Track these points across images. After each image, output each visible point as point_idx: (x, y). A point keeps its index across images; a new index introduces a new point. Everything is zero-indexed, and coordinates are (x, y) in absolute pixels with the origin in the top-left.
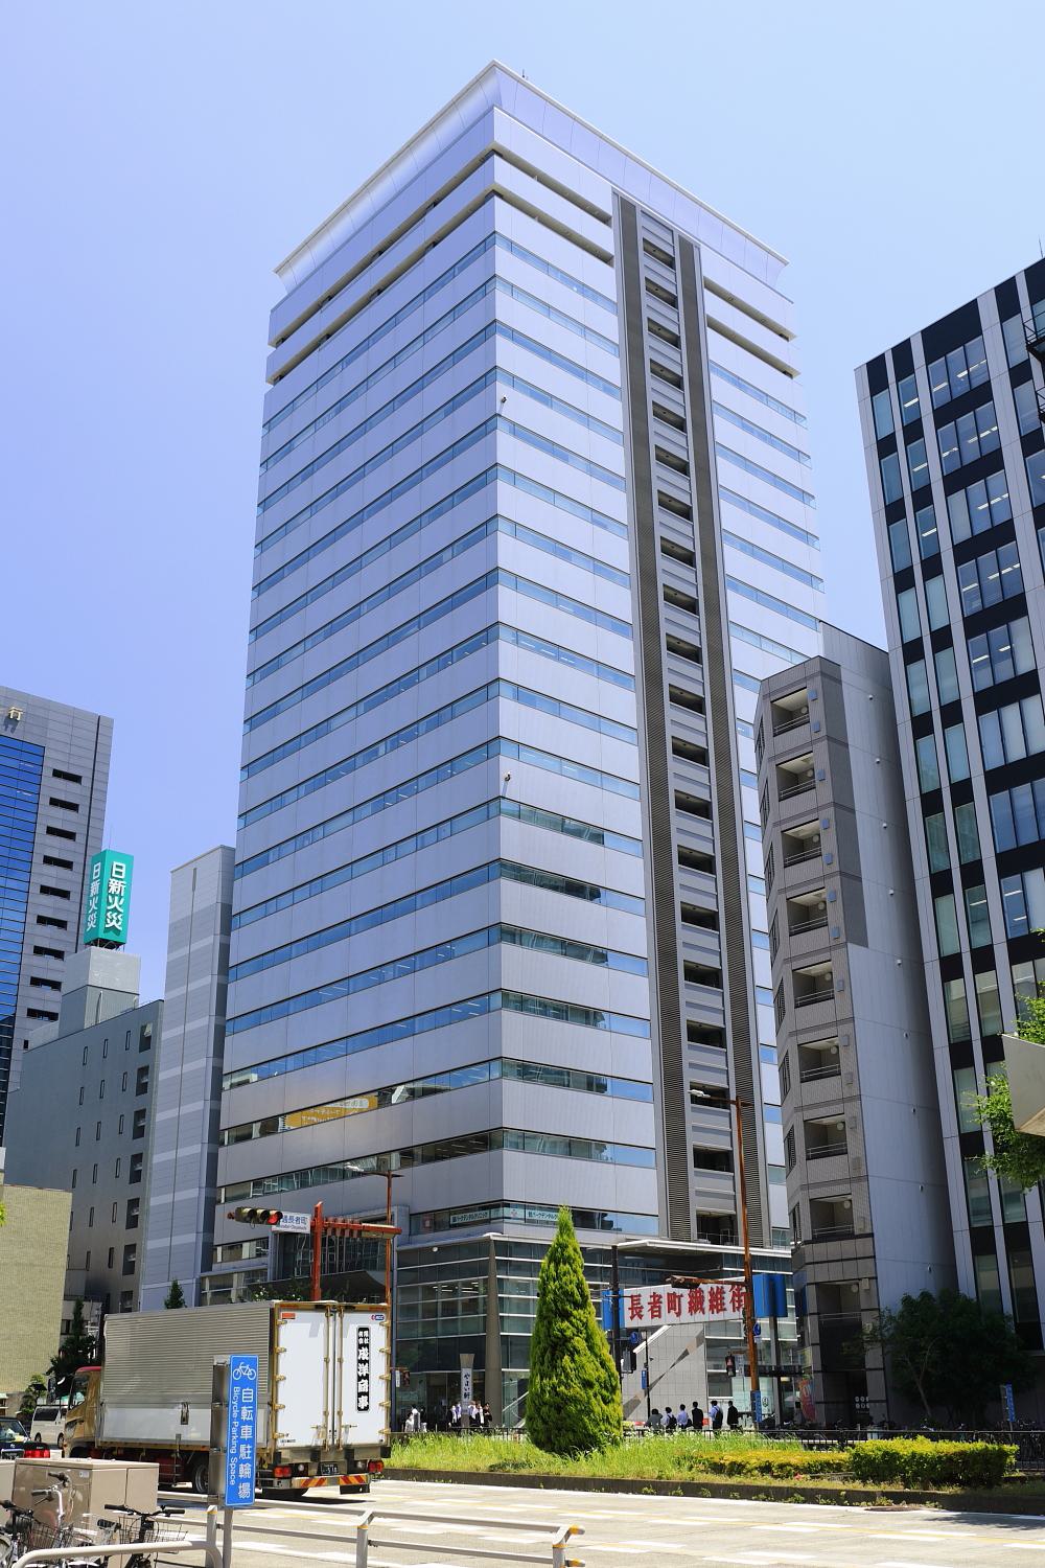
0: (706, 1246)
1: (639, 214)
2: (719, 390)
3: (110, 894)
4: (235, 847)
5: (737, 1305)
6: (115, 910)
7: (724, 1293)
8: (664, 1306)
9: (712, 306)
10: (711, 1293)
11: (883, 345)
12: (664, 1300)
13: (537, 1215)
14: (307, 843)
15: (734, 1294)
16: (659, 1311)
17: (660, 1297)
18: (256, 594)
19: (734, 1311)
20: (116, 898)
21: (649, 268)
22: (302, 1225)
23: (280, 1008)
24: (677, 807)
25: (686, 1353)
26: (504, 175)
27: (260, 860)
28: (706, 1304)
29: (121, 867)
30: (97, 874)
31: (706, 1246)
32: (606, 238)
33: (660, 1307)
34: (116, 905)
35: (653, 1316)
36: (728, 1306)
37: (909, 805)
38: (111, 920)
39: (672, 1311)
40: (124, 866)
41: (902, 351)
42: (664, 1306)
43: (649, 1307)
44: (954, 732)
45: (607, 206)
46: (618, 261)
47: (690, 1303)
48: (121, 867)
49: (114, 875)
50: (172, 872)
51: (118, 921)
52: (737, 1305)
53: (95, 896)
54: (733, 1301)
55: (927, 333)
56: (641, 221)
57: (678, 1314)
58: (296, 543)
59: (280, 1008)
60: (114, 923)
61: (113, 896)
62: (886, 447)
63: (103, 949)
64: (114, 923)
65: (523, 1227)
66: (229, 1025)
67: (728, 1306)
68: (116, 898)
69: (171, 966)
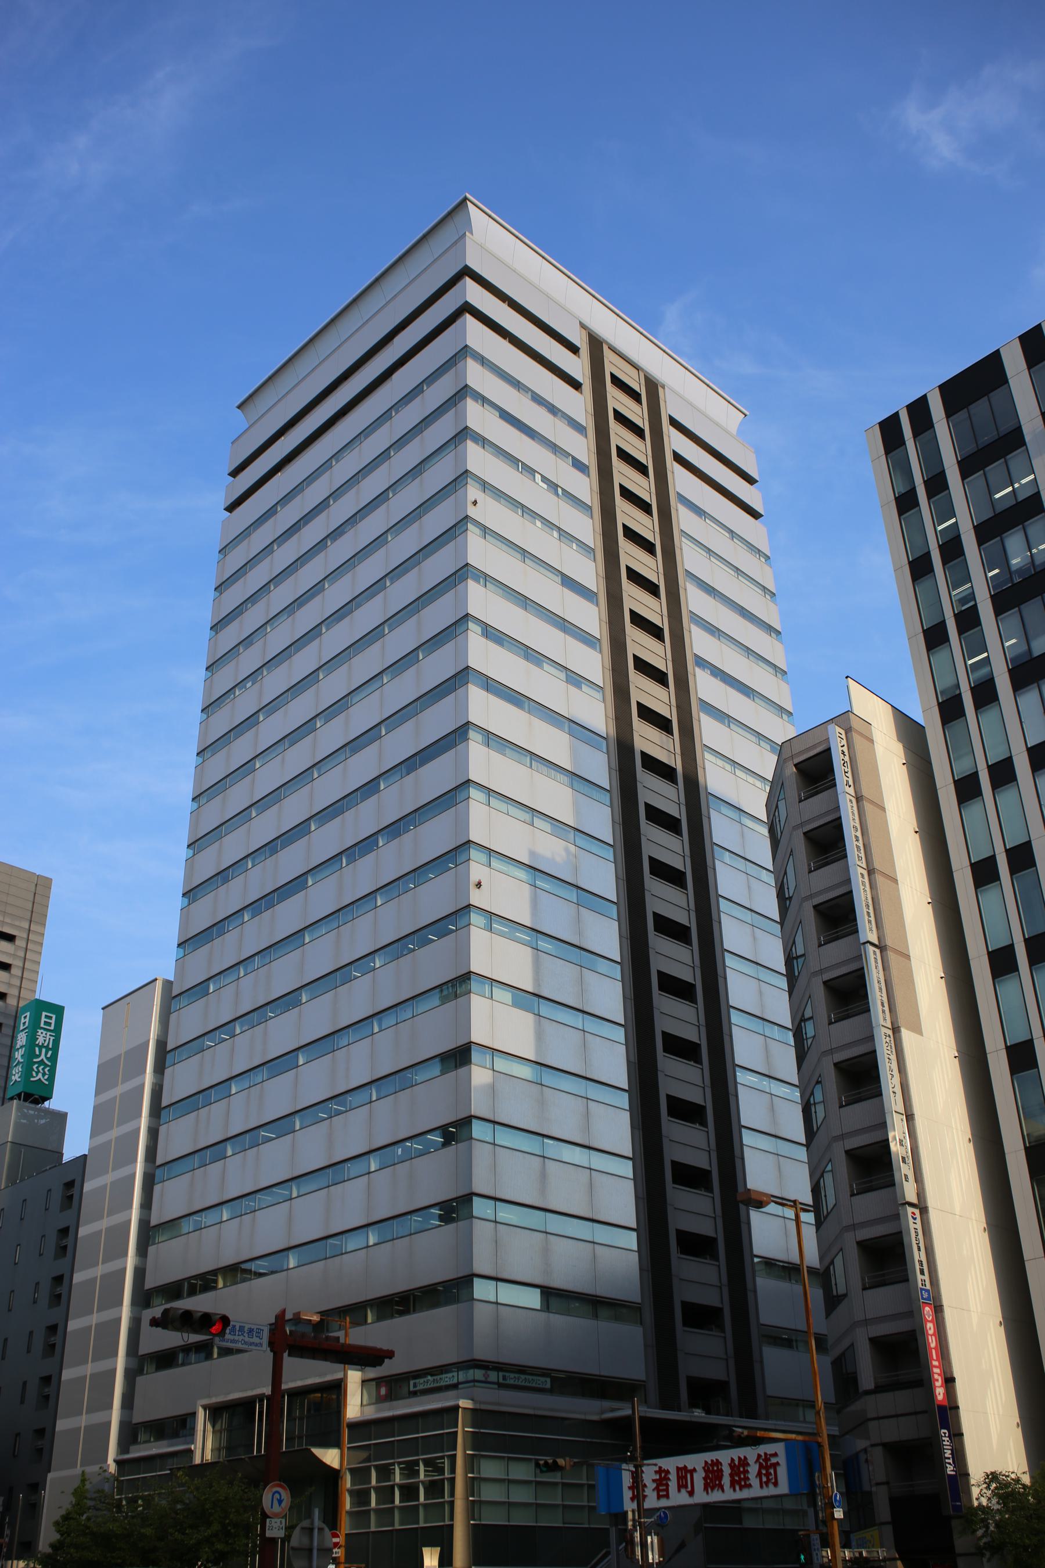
0: (698, 1415)
1: (605, 347)
2: (683, 519)
3: (38, 1045)
4: (173, 980)
5: (764, 1479)
6: (42, 1062)
7: (748, 1465)
8: (673, 1484)
9: (675, 441)
10: (732, 1465)
11: (898, 402)
12: (673, 1477)
13: (512, 1379)
14: (249, 970)
15: (761, 1466)
16: (667, 1490)
17: (668, 1472)
18: (205, 716)
19: (761, 1487)
20: (44, 1050)
21: (616, 399)
22: (256, 1340)
23: (215, 1150)
24: (655, 931)
25: (682, 1546)
26: (473, 293)
27: (200, 989)
28: (726, 1481)
29: (51, 1018)
30: (24, 1023)
31: (698, 1415)
32: (578, 367)
33: (667, 1485)
34: (43, 1056)
35: (659, 1497)
36: (754, 1481)
37: (957, 877)
38: (37, 1073)
39: (683, 1491)
40: (54, 1017)
41: (919, 409)
42: (673, 1484)
43: (654, 1485)
44: (1007, 795)
45: (578, 338)
46: (587, 387)
47: (705, 1479)
48: (51, 1018)
49: (42, 1025)
50: (103, 1009)
51: (44, 1074)
52: (764, 1479)
53: (22, 1047)
54: (759, 1474)
55: (945, 389)
56: (607, 354)
57: (691, 1493)
58: (238, 797)
59: (215, 1150)
60: (40, 1076)
61: (41, 1047)
62: (906, 503)
63: (27, 1104)
64: (40, 1076)
65: (497, 1391)
66: (158, 1172)
67: (754, 1481)
68: (44, 1050)
69: (97, 1109)
